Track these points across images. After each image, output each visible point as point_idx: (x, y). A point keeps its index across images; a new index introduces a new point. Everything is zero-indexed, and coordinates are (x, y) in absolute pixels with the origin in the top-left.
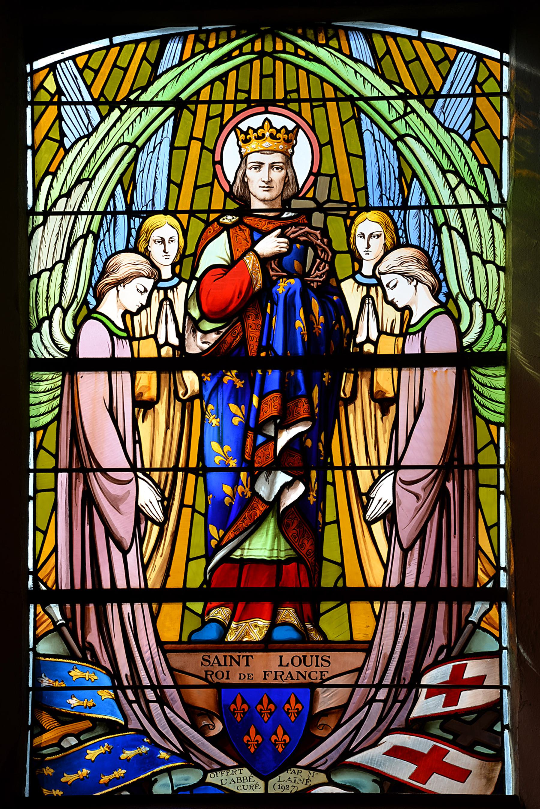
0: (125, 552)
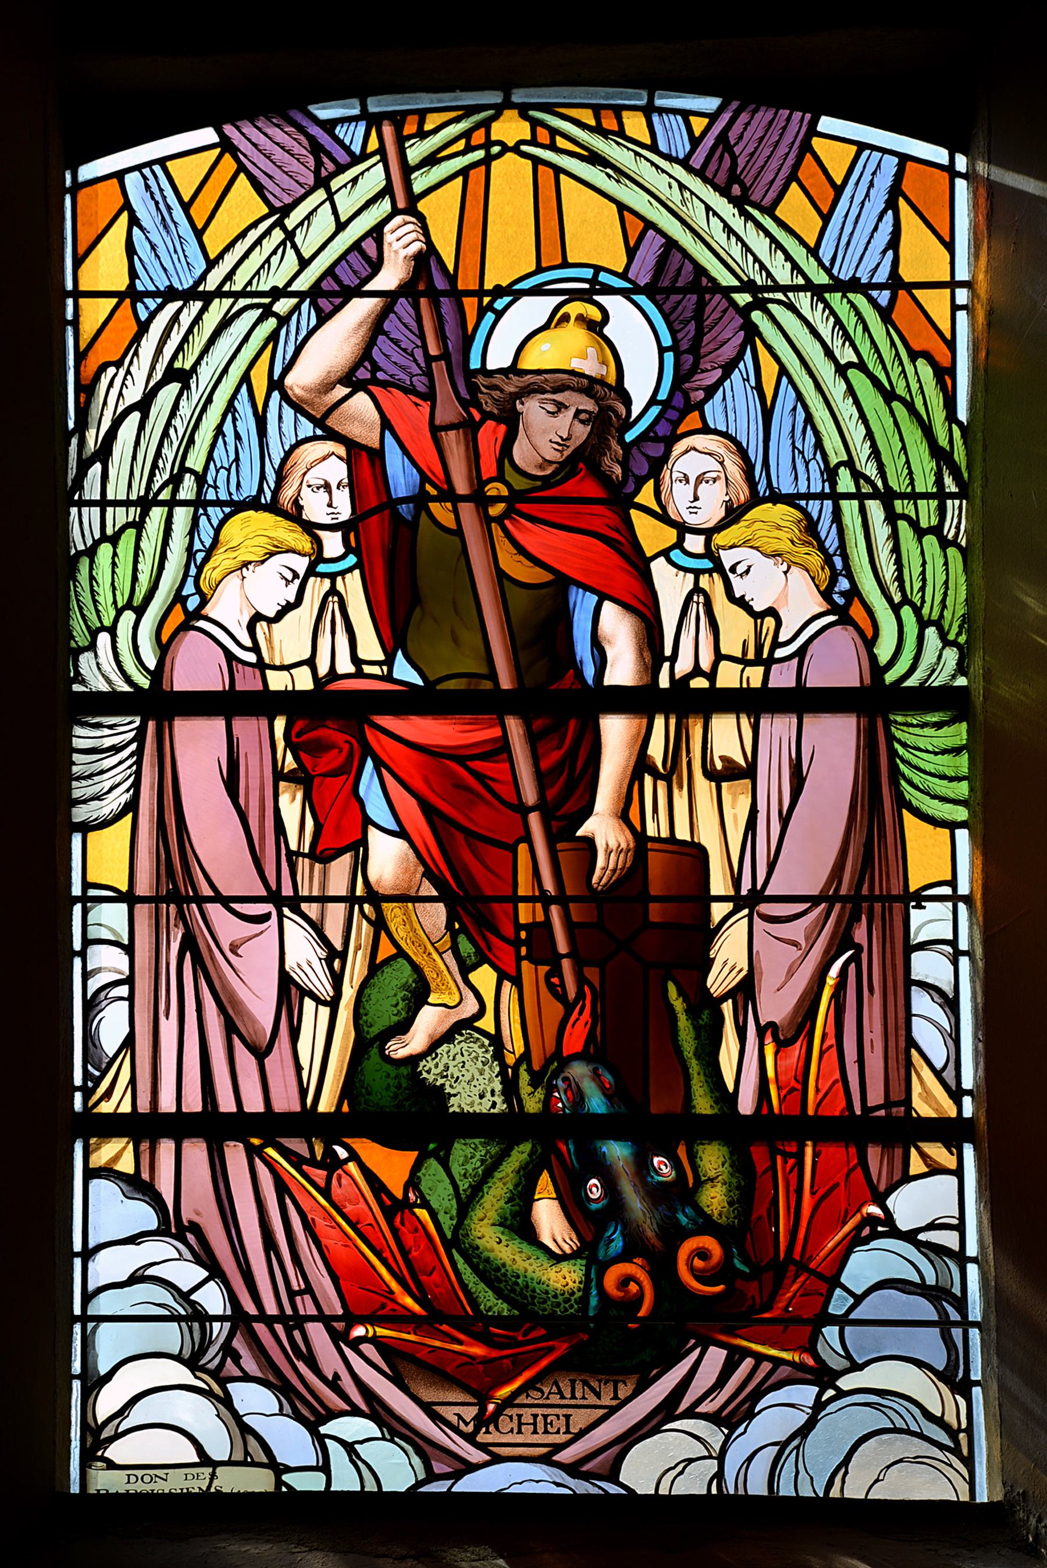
0: (261, 1054)
